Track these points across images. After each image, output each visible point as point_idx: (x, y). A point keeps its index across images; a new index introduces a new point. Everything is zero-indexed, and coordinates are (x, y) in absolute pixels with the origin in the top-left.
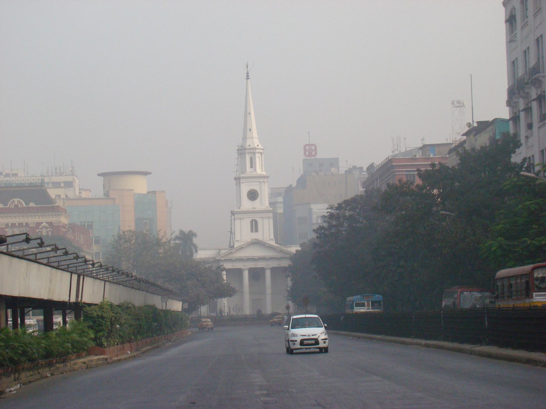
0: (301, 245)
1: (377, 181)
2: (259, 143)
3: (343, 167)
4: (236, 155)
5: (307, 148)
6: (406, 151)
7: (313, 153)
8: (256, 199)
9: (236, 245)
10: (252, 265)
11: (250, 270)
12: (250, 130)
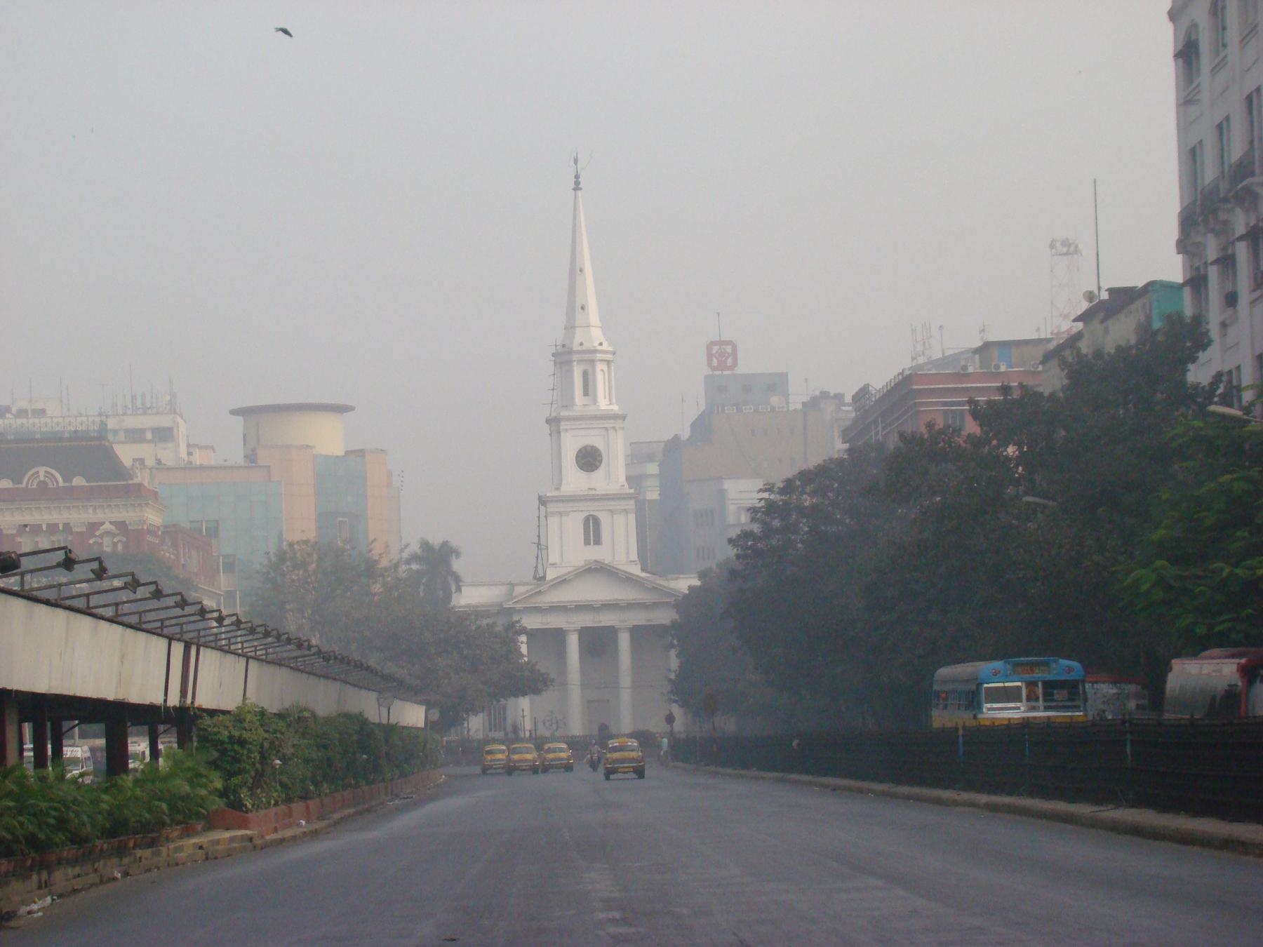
0: (702, 575)
2: (602, 339)
3: (798, 396)
6: (944, 358)
7: (729, 362)
8: (597, 468)
9: (551, 574)
10: (588, 620)
11: (583, 632)
12: (583, 308)
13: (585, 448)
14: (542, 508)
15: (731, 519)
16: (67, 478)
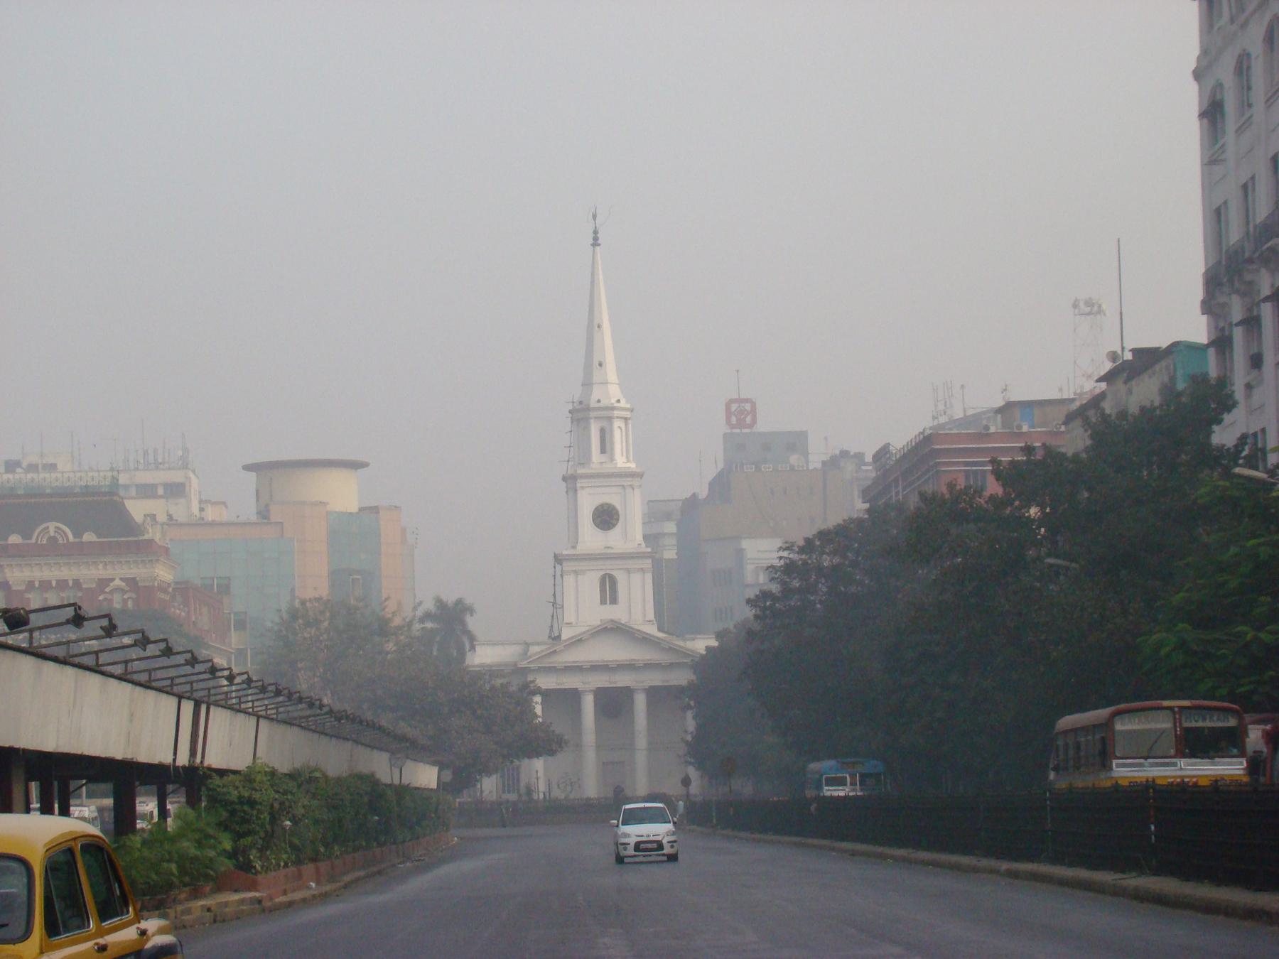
0: (719, 636)
1: (897, 487)
5: (734, 407)
7: (748, 420)
8: (614, 526)
9: (566, 634)
10: (602, 681)
12: (600, 365)
14: (558, 567)
15: (749, 579)
16: (78, 534)
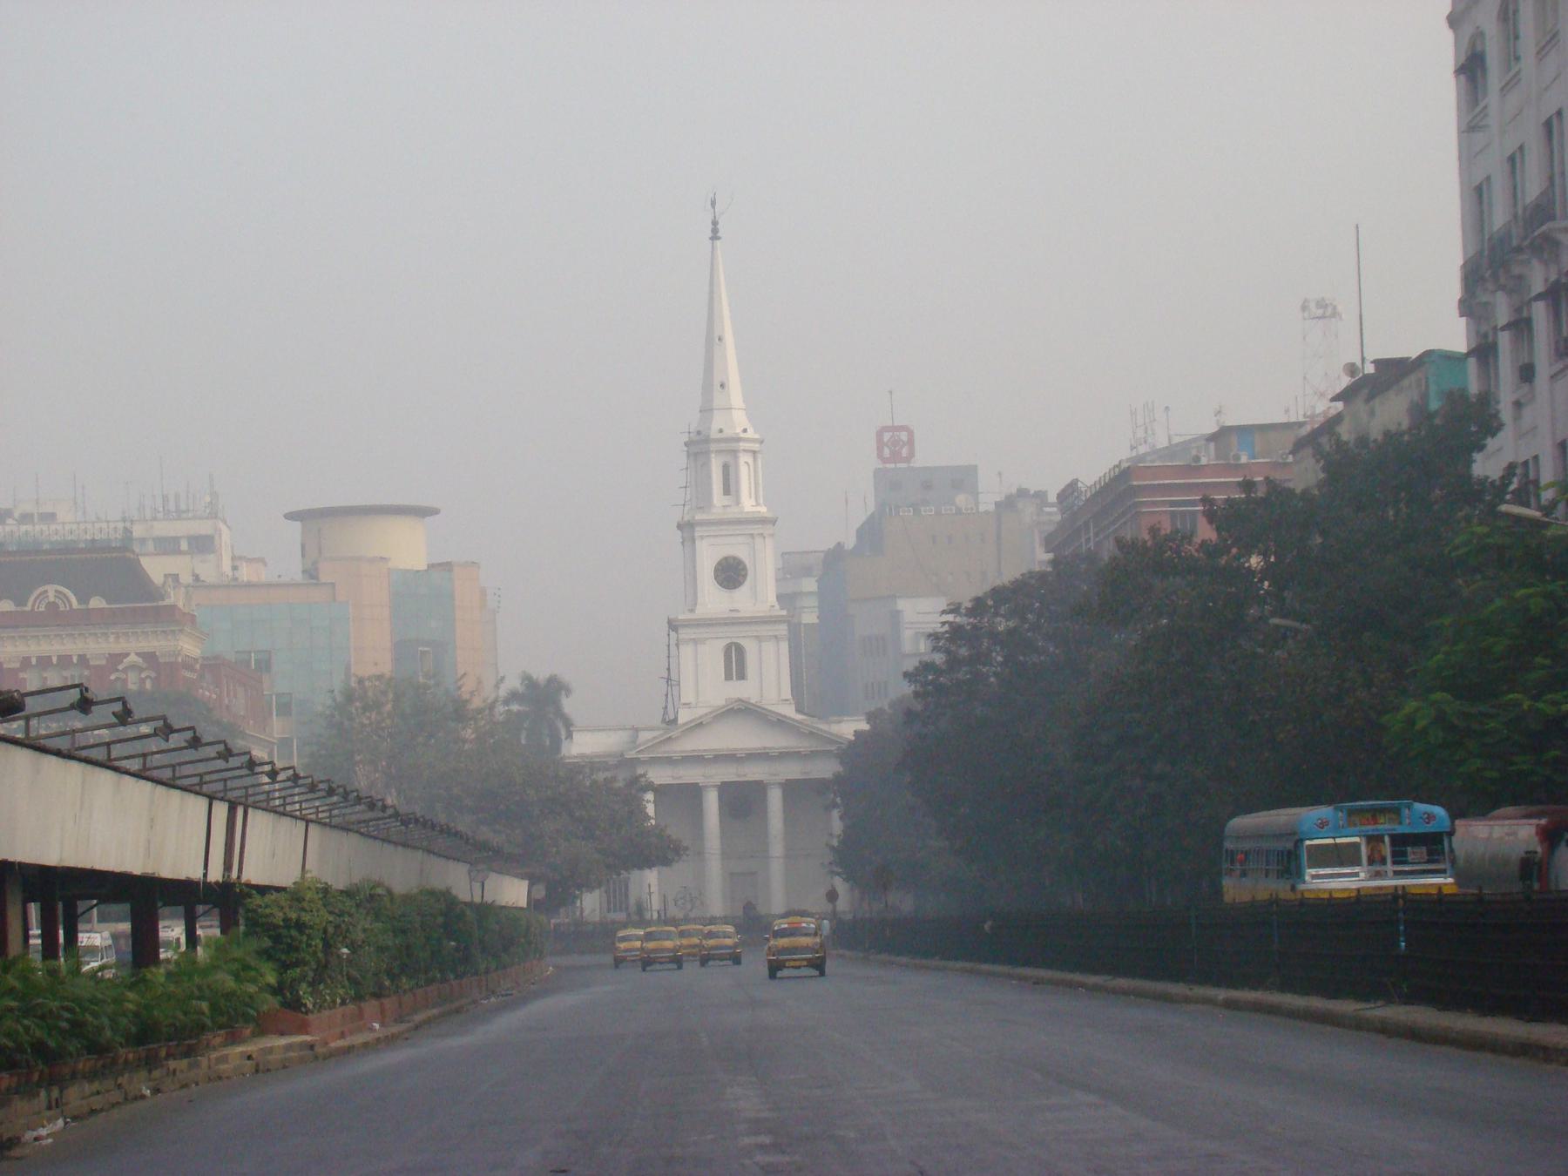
0: (871, 717)
3: (989, 495)
4: (682, 460)
7: (904, 452)
9: (684, 717)
10: (729, 773)
11: (724, 788)
13: (726, 559)
14: (673, 634)
